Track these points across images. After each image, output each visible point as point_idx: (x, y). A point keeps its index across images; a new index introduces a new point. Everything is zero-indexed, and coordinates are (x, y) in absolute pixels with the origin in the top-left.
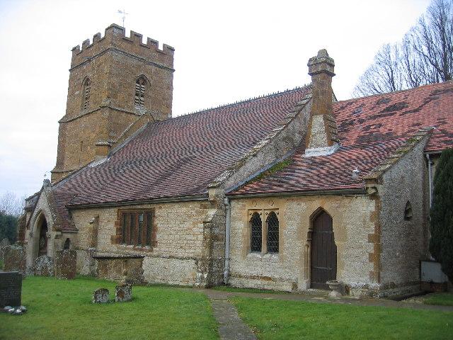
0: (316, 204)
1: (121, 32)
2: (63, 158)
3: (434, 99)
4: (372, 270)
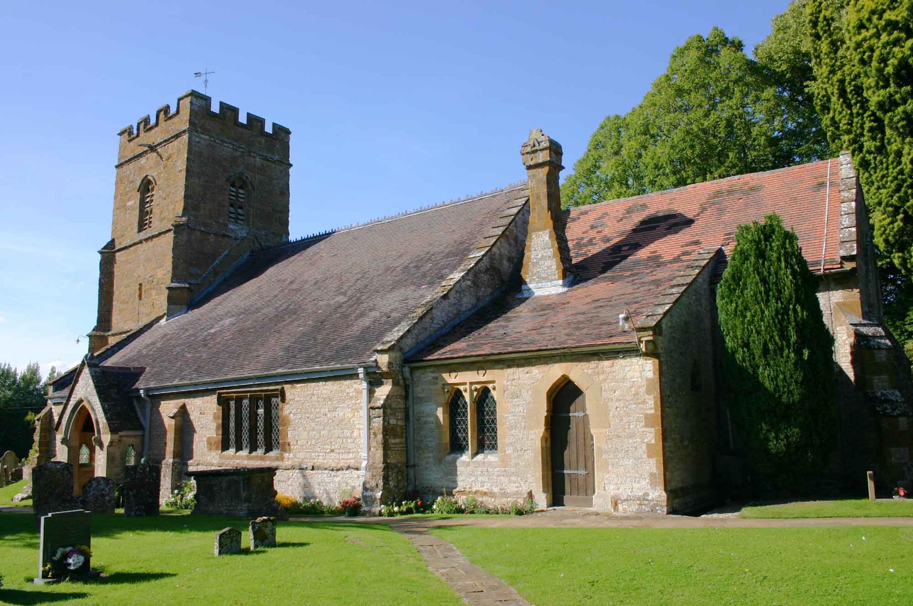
0: (555, 372)
1: (204, 102)
2: (109, 311)
3: (714, 204)
4: (654, 470)
